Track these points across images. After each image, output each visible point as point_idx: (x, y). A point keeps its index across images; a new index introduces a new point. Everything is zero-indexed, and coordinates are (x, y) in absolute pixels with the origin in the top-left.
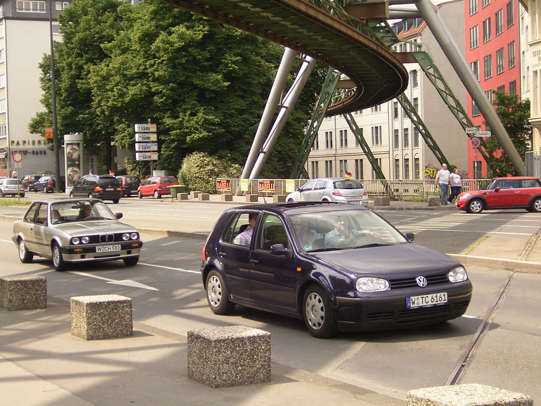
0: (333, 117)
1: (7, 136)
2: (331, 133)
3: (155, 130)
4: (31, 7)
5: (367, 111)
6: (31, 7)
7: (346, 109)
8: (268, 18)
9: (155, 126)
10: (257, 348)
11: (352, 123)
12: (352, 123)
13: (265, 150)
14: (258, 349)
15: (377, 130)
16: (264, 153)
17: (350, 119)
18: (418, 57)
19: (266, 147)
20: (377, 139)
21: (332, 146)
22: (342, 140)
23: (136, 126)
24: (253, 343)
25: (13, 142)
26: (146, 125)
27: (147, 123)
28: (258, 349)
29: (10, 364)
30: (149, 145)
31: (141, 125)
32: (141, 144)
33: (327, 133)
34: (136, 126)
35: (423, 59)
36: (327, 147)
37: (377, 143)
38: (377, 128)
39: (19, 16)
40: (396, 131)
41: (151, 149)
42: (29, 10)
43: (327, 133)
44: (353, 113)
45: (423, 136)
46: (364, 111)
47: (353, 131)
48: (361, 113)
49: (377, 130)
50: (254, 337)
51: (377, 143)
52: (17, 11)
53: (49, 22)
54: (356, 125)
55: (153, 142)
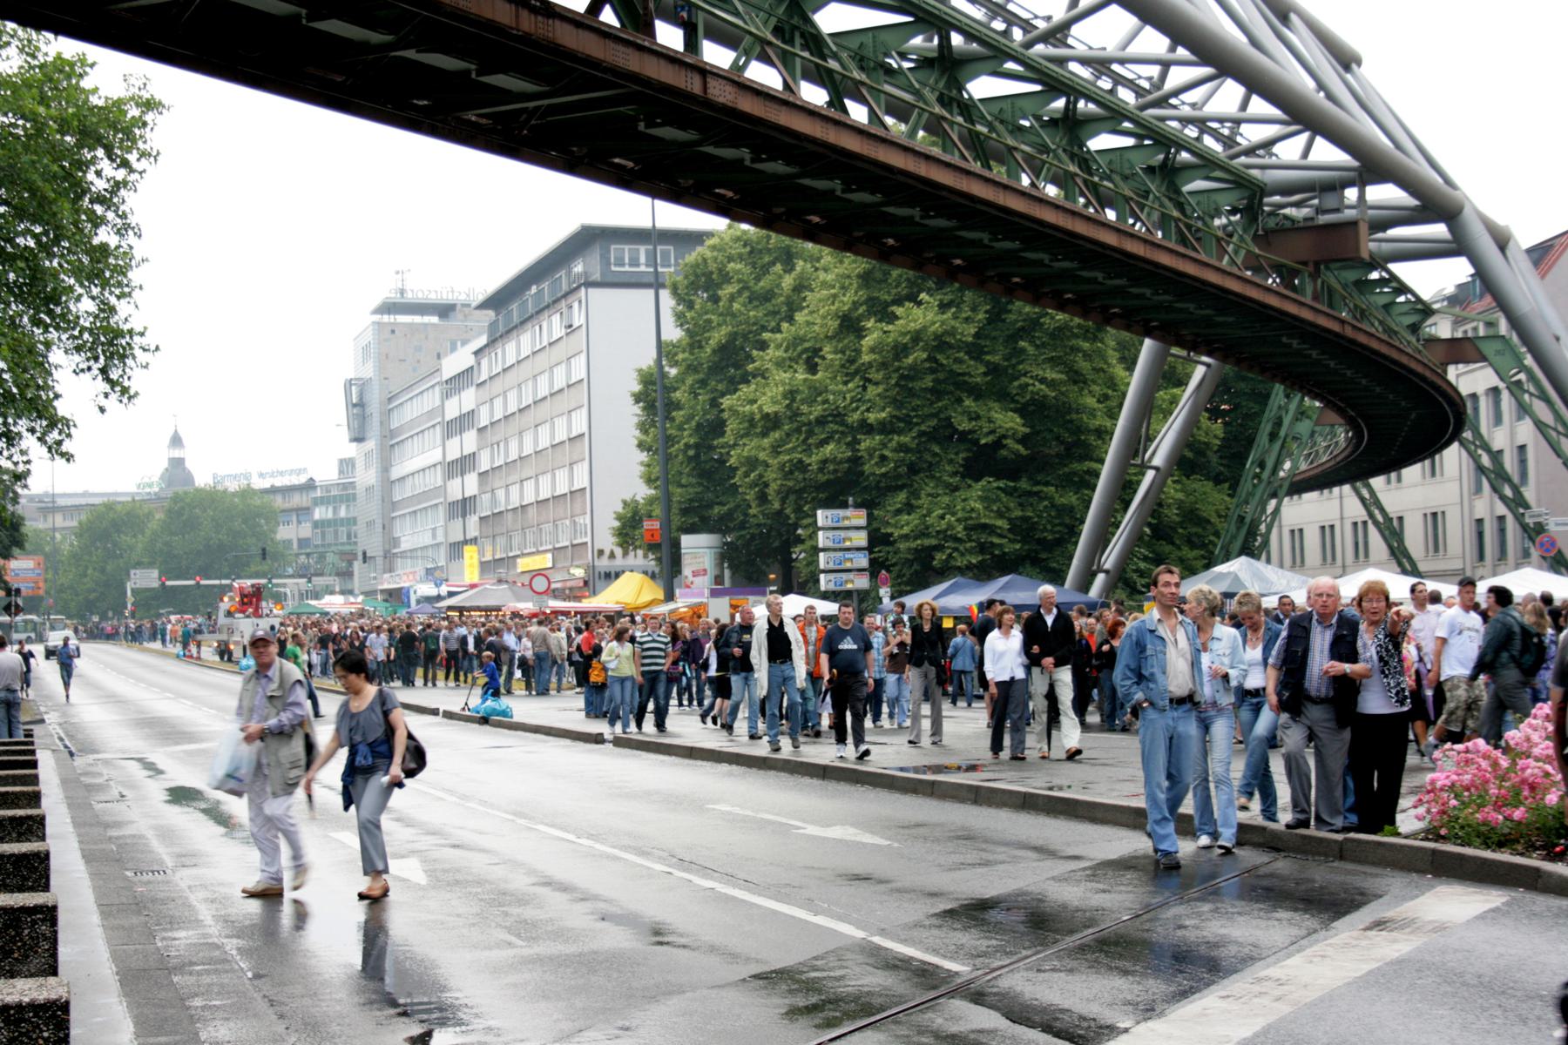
0: (1336, 490)
1: (588, 539)
2: (1332, 527)
3: (862, 522)
4: (643, 259)
5: (1412, 473)
6: (643, 259)
7: (1354, 469)
8: (1040, 263)
9: (863, 513)
10: (26, 1034)
11: (1371, 502)
12: (1371, 502)
13: (1107, 566)
14: (30, 1038)
15: (1435, 519)
16: (1107, 572)
17: (1367, 496)
18: (1488, 348)
19: (1110, 559)
20: (1436, 542)
21: (1334, 558)
22: (1356, 544)
23: (819, 512)
24: (17, 1022)
25: (601, 552)
26: (841, 513)
27: (844, 505)
28: (30, 1038)
29: (868, 1033)
30: (849, 555)
31: (829, 512)
32: (832, 554)
33: (1323, 528)
34: (819, 512)
35: (1498, 353)
36: (1481, 557)
37: (1436, 549)
38: (1434, 515)
39: (616, 280)
40: (1480, 522)
41: (856, 565)
42: (638, 265)
43: (1323, 528)
44: (1377, 482)
45: (1381, 531)
46: (1406, 472)
47: (1376, 523)
48: (1399, 480)
49: (1435, 519)
50: (19, 1007)
51: (1436, 549)
52: (614, 268)
53: (651, 292)
54: (1382, 510)
55: (859, 549)
